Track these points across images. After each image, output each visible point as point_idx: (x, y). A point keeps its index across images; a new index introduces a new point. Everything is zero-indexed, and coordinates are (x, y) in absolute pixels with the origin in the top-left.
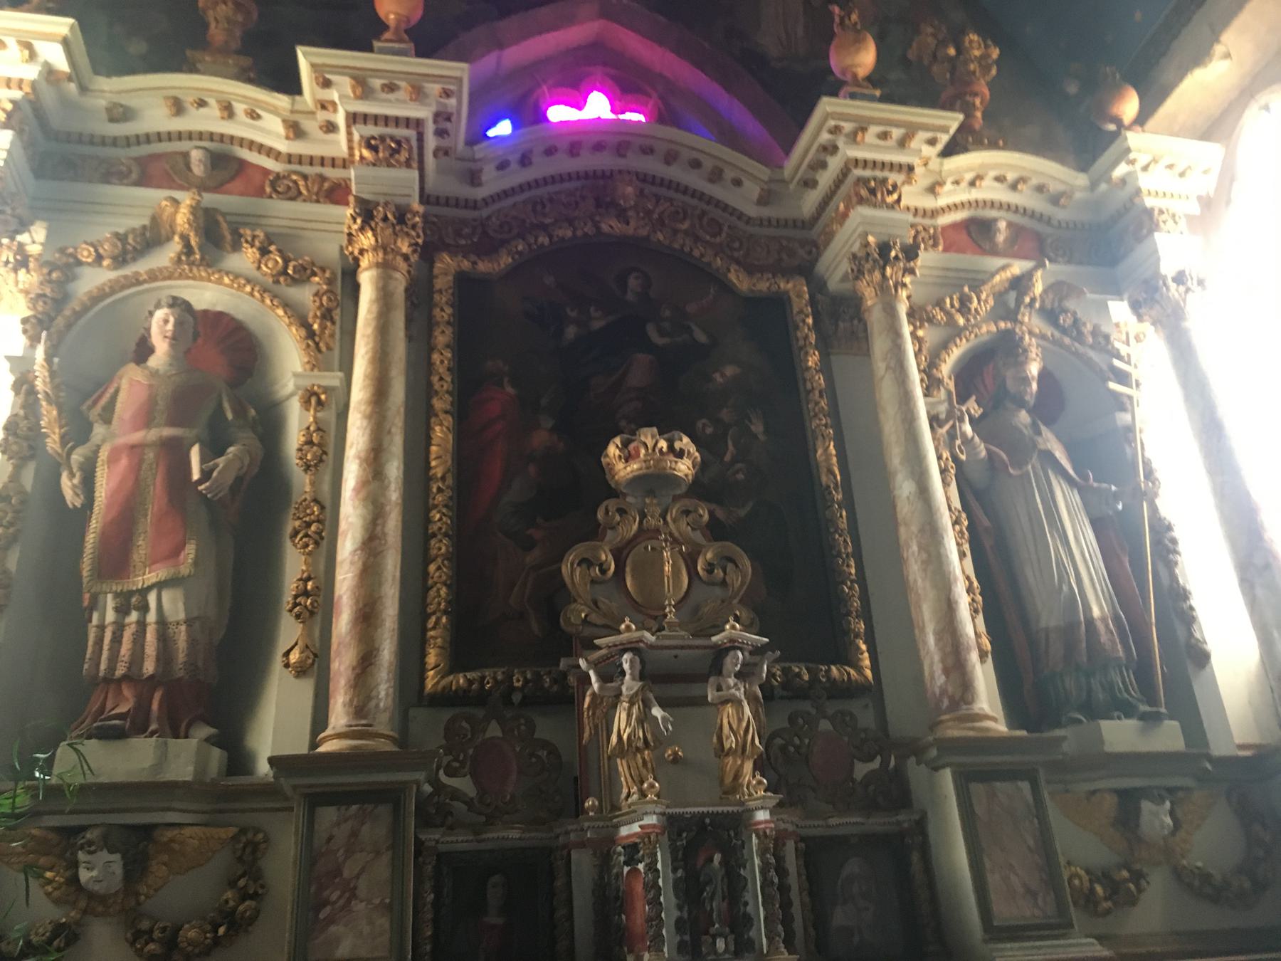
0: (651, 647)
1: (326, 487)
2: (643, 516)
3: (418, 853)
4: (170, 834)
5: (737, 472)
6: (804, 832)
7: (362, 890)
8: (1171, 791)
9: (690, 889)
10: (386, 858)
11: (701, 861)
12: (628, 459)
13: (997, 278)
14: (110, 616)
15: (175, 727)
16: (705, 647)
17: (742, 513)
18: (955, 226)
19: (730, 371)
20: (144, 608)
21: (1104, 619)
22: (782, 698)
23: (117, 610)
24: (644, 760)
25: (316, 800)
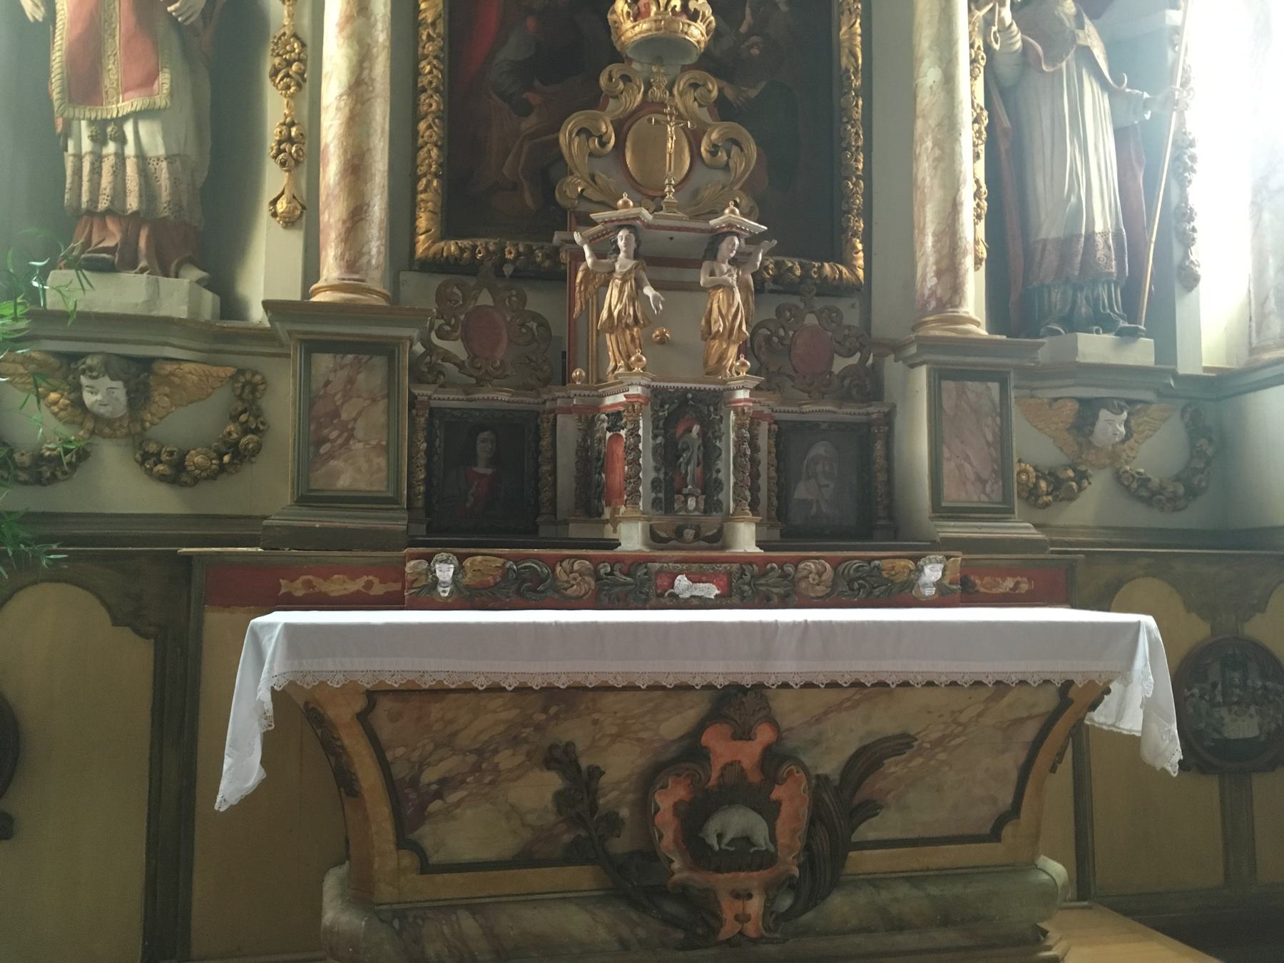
0: (649, 226)
1: (306, 21)
2: (649, 86)
3: (412, 406)
4: (169, 368)
5: (752, 47)
6: (778, 416)
7: (359, 433)
8: (1130, 402)
9: (669, 454)
10: (382, 405)
11: (680, 431)
14: (87, 145)
15: (164, 266)
16: (702, 231)
17: (753, 93)
20: (122, 140)
21: (1104, 234)
22: (772, 291)
23: (93, 138)
24: (632, 337)
25: (312, 346)
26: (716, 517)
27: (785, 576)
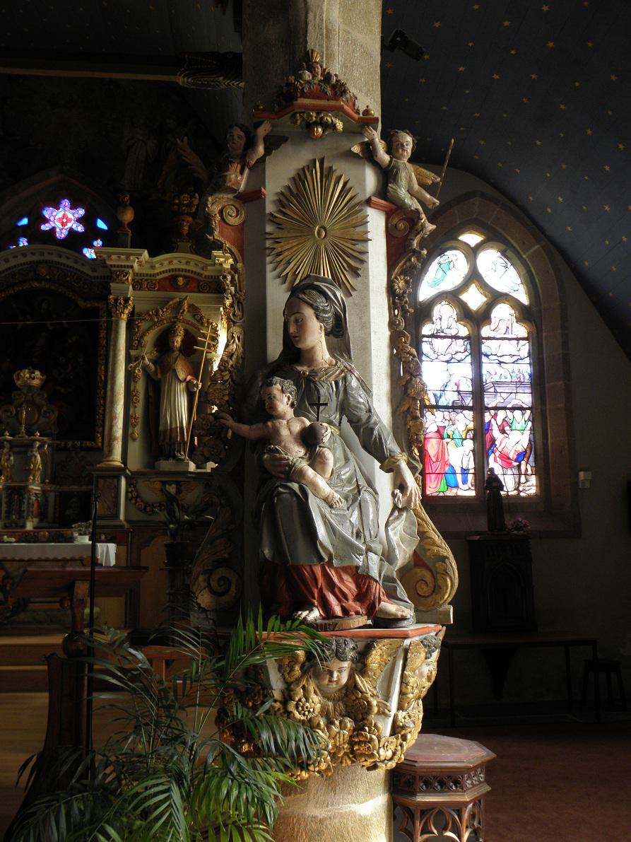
8: (177, 482)
12: (18, 379)
13: (171, 303)
18: (165, 279)
19: (74, 338)
26: (22, 520)
27: (34, 535)
